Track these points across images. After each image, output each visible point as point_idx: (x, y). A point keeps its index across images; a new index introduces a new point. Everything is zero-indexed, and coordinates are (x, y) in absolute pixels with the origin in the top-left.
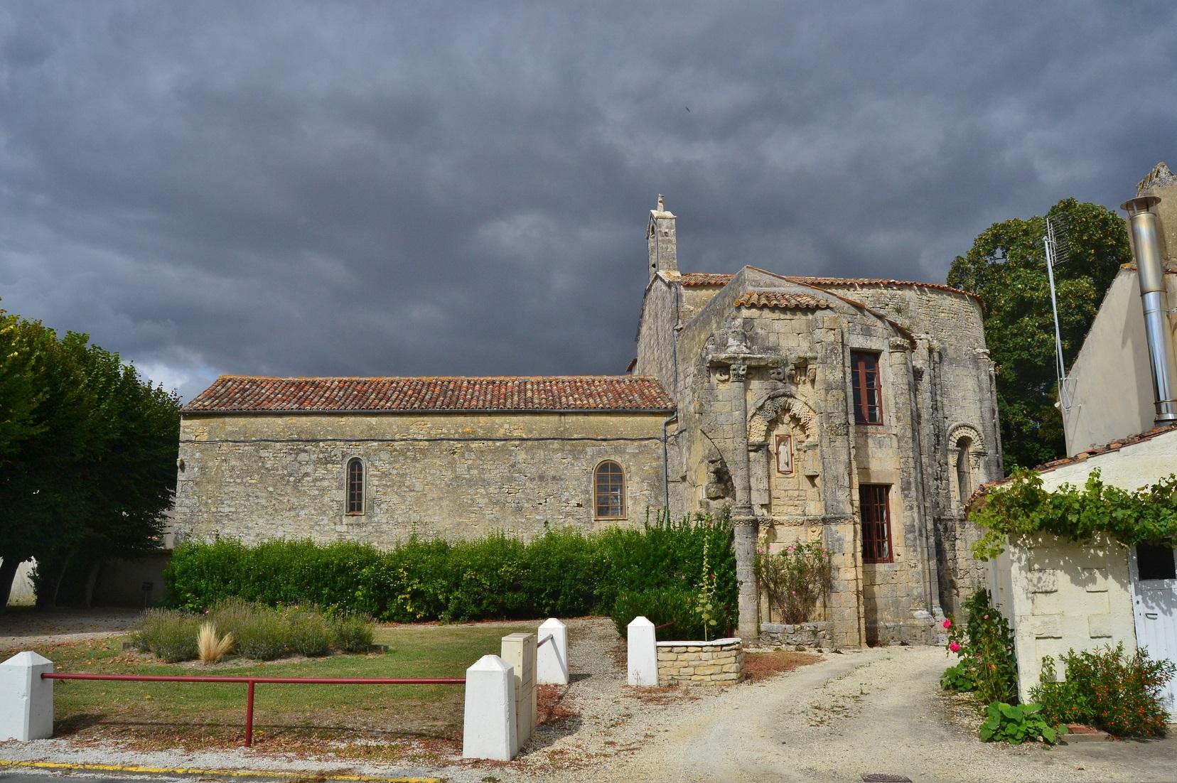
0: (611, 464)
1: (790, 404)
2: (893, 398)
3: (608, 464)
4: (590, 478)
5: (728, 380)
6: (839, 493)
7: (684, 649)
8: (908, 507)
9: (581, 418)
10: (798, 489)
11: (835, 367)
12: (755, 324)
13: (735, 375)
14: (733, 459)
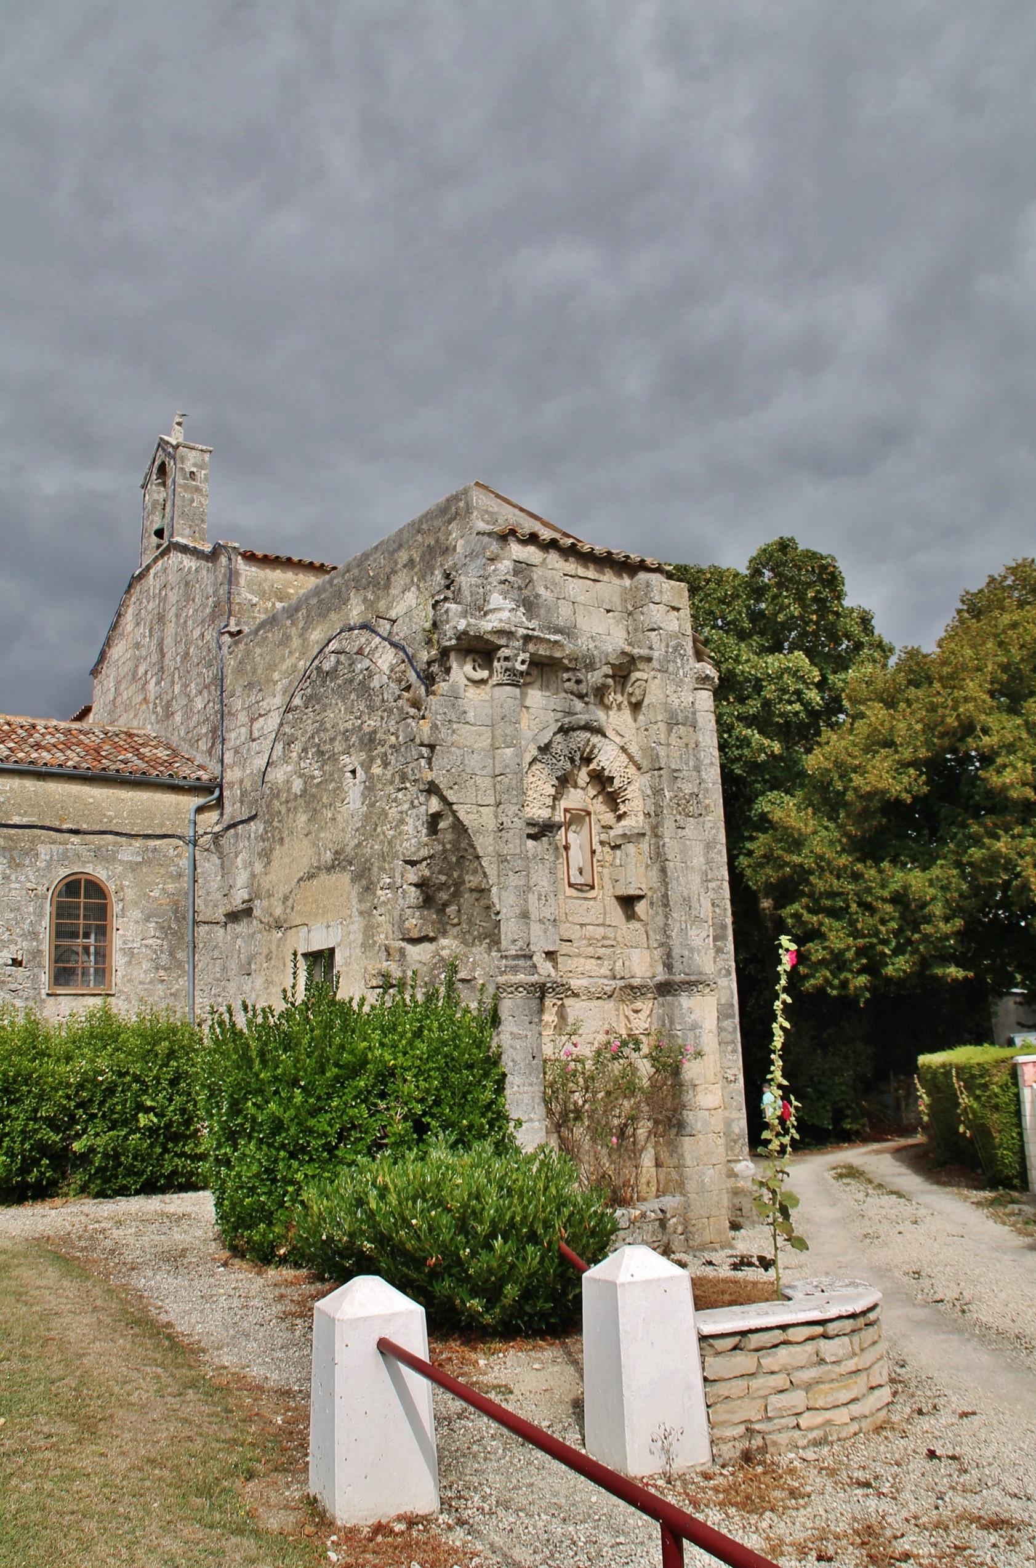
0: (87, 881)
1: (594, 746)
3: (78, 881)
4: (41, 907)
5: (483, 682)
7: (777, 1336)
8: (724, 972)
9: (30, 784)
10: (603, 925)
12: (535, 577)
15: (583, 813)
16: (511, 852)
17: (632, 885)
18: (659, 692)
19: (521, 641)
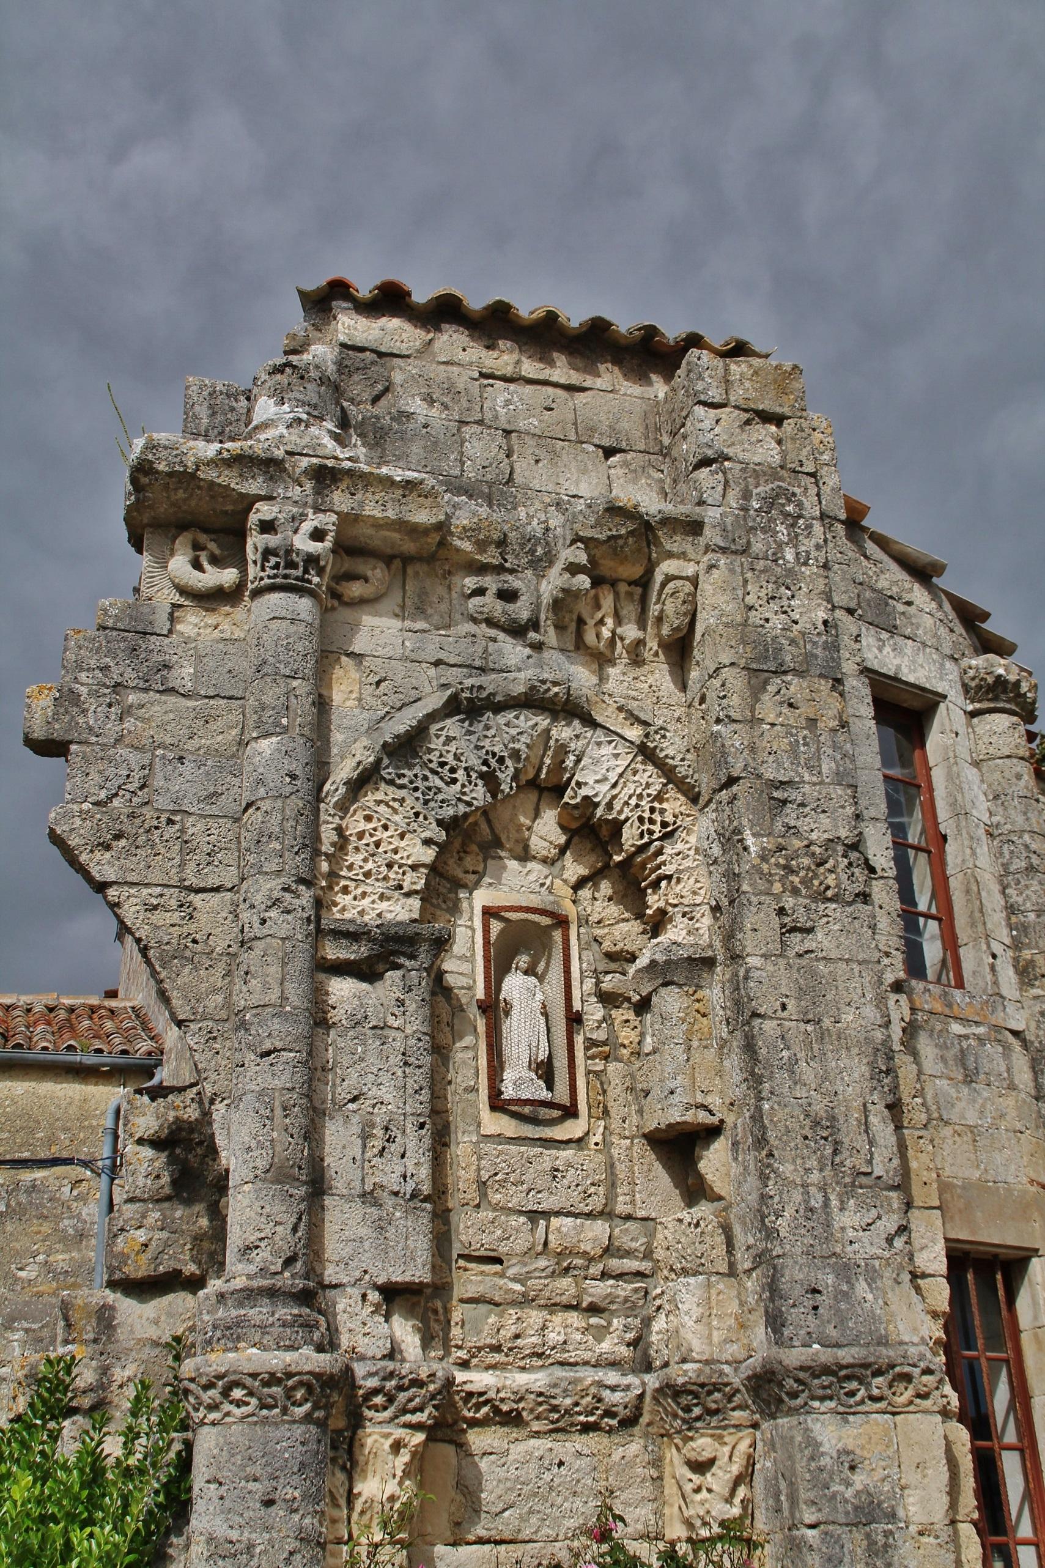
2: (996, 888)
6: (848, 1219)
10: (606, 1214)
11: (790, 572)
13: (268, 553)
14: (228, 1003)
15: (545, 921)
16: (255, 1000)
17: (675, 1099)
18: (721, 599)
19: (309, 486)
